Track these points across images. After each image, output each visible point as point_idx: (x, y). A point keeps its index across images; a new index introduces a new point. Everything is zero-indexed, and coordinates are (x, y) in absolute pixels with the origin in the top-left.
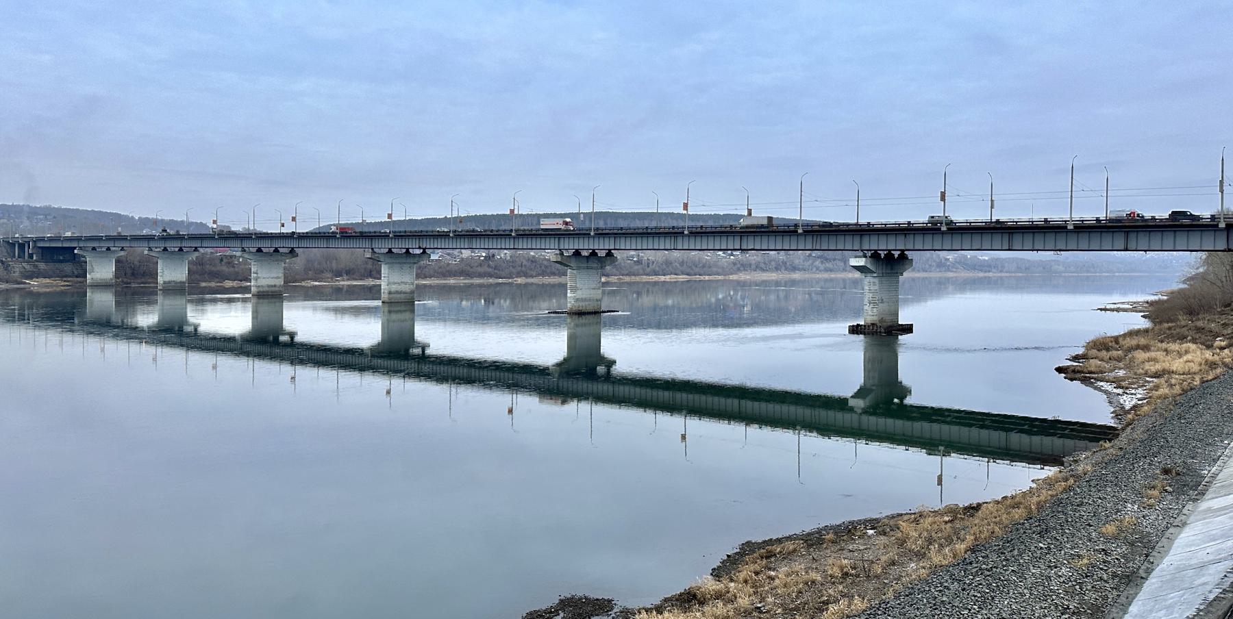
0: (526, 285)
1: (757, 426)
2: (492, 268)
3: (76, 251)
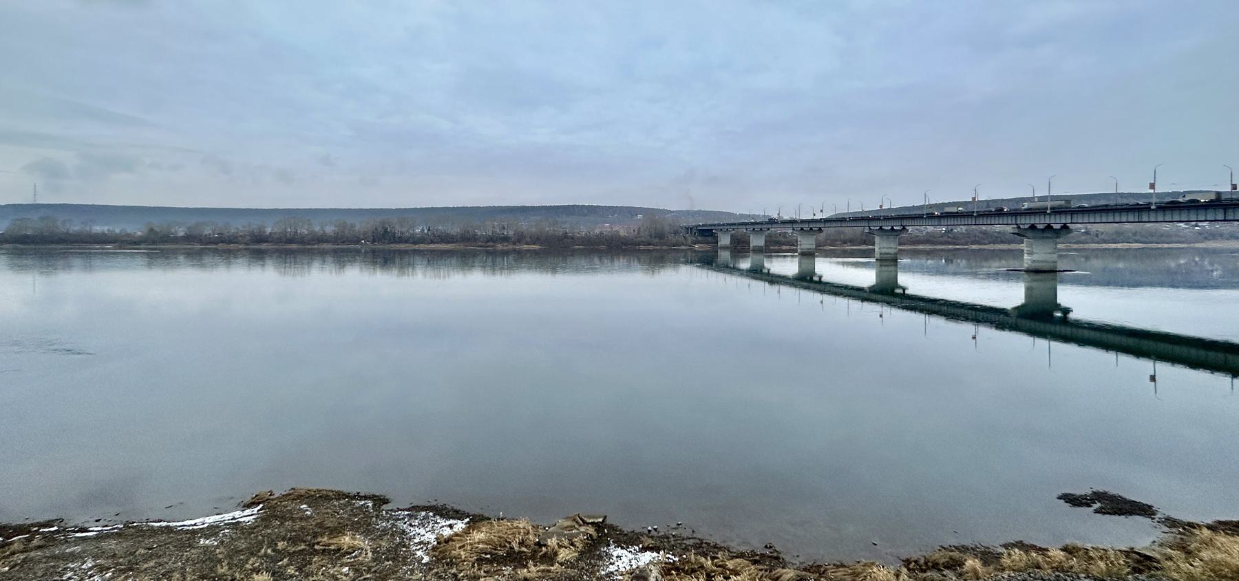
2: (951, 238)
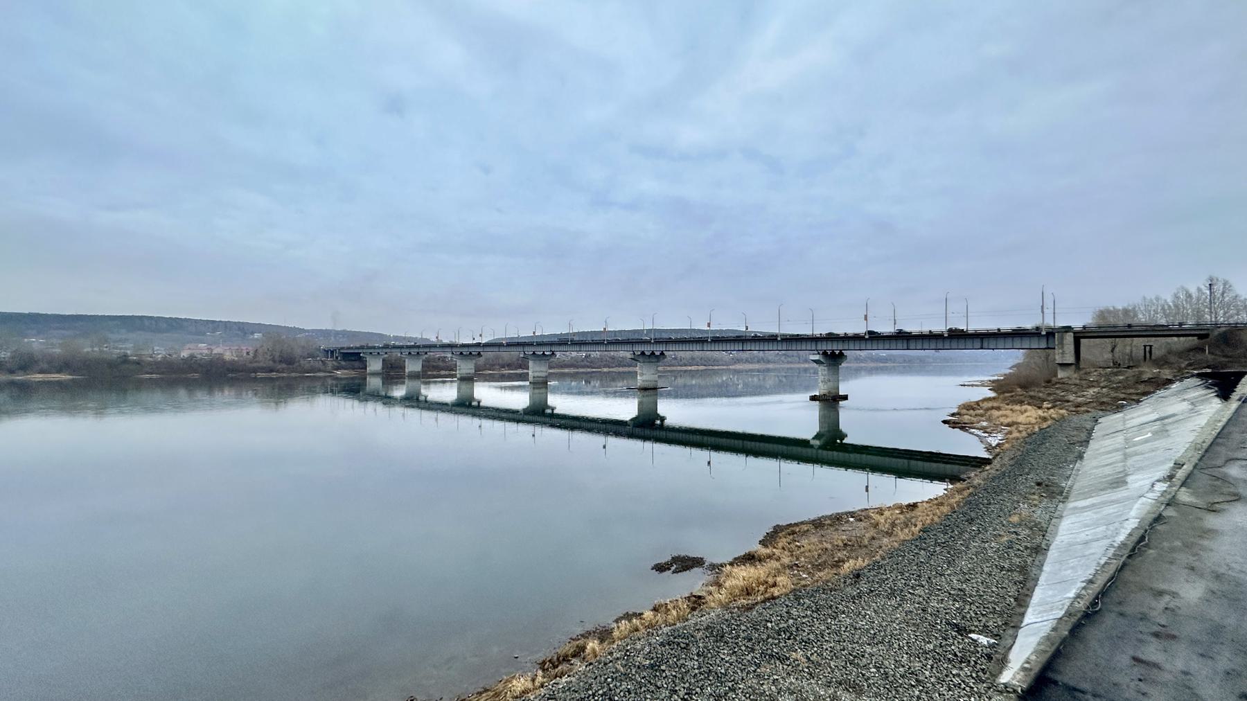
0: (609, 372)
1: (735, 454)
3: (361, 355)
